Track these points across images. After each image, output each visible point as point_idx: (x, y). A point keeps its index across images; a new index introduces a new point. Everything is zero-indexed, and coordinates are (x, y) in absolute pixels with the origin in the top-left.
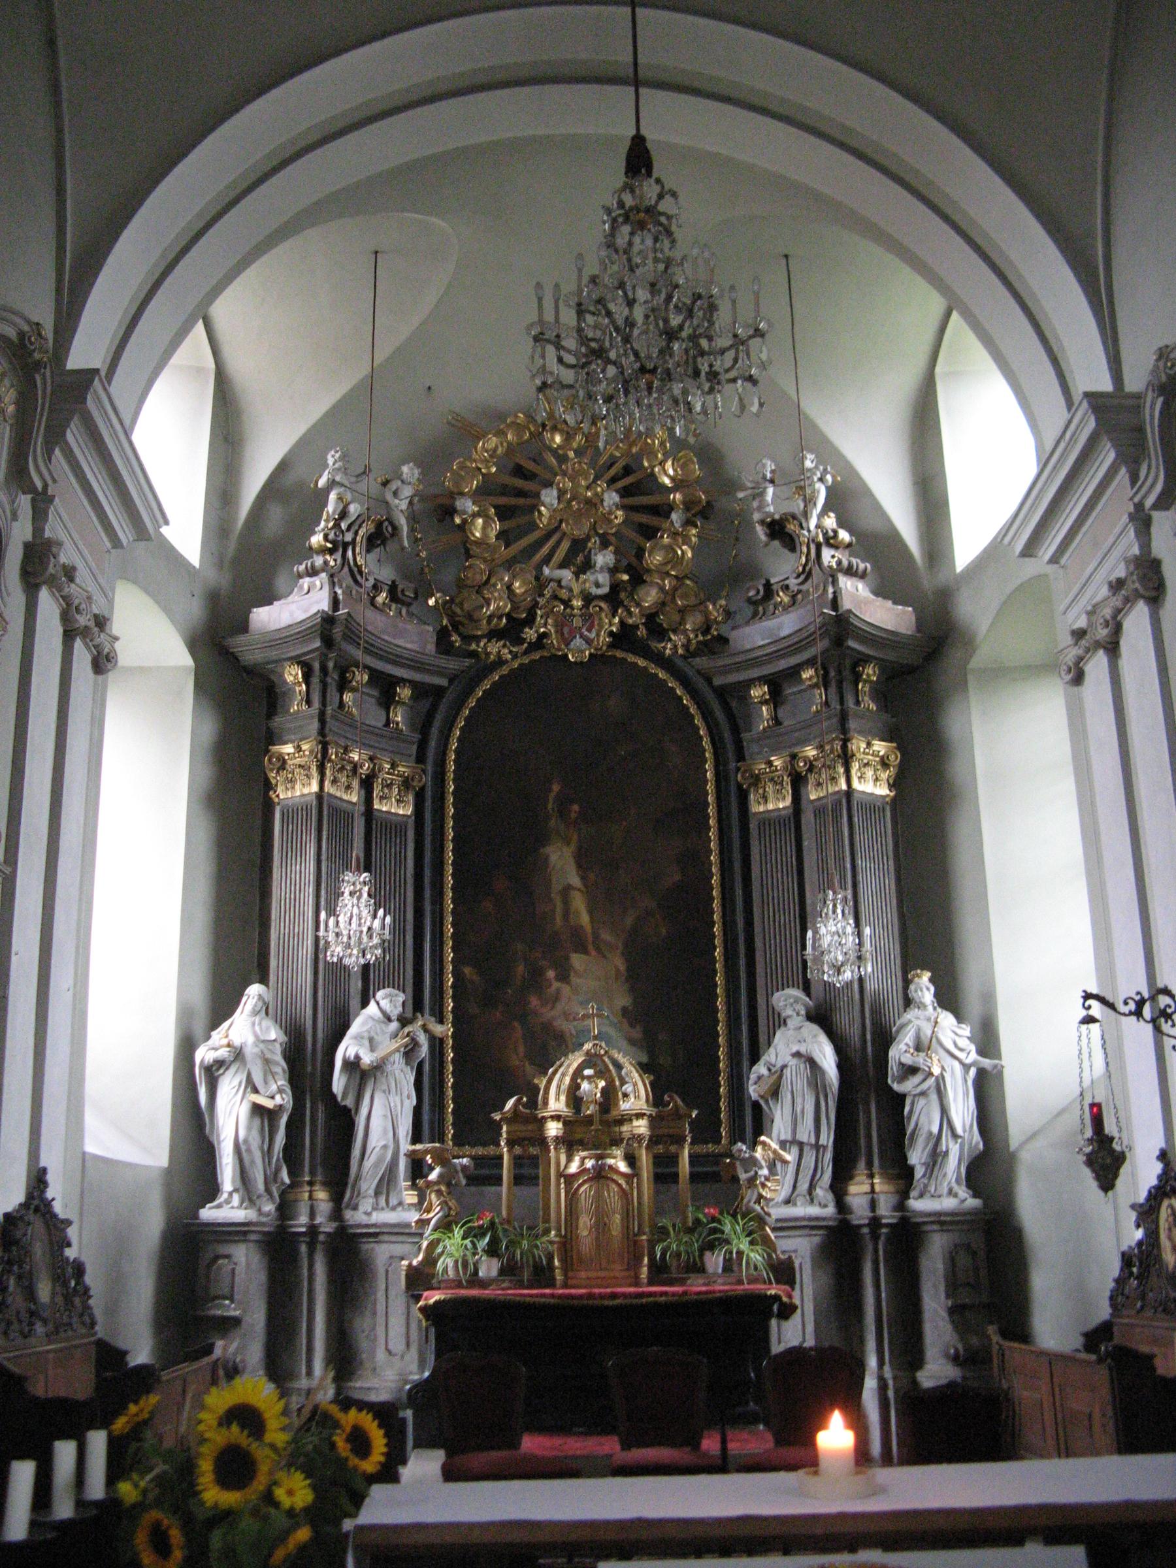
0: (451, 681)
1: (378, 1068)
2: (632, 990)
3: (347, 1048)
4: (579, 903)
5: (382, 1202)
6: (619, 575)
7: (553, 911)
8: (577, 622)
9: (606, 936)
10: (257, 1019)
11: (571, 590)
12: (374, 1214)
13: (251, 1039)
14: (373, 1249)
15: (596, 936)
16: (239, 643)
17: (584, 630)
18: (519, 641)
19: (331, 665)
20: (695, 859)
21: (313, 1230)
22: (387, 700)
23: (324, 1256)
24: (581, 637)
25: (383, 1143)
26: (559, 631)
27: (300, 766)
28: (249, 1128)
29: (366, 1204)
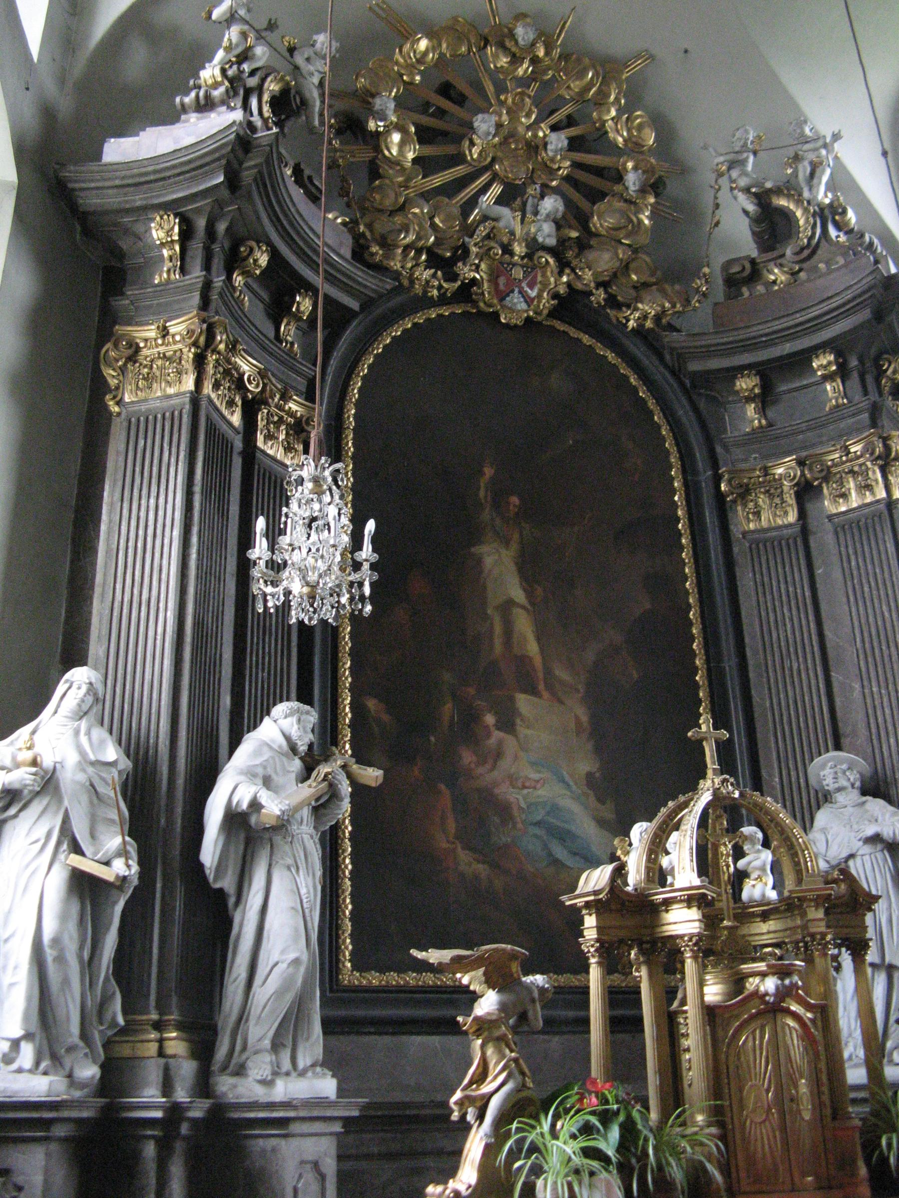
0: (363, 308)
1: (282, 826)
2: (598, 750)
3: (232, 788)
4: (524, 624)
5: (286, 1065)
6: (566, 231)
7: (491, 630)
8: (518, 273)
9: (562, 673)
10: (84, 724)
11: (512, 233)
12: (280, 1084)
13: (72, 758)
14: (274, 1150)
15: (548, 672)
16: (80, 177)
17: (524, 285)
18: (451, 277)
19: (222, 227)
20: (666, 584)
21: (175, 1112)
22: (279, 308)
23: (186, 1163)
24: (520, 292)
25: (292, 956)
26: (494, 277)
27: (164, 357)
28: (63, 918)
29: (260, 1066)
